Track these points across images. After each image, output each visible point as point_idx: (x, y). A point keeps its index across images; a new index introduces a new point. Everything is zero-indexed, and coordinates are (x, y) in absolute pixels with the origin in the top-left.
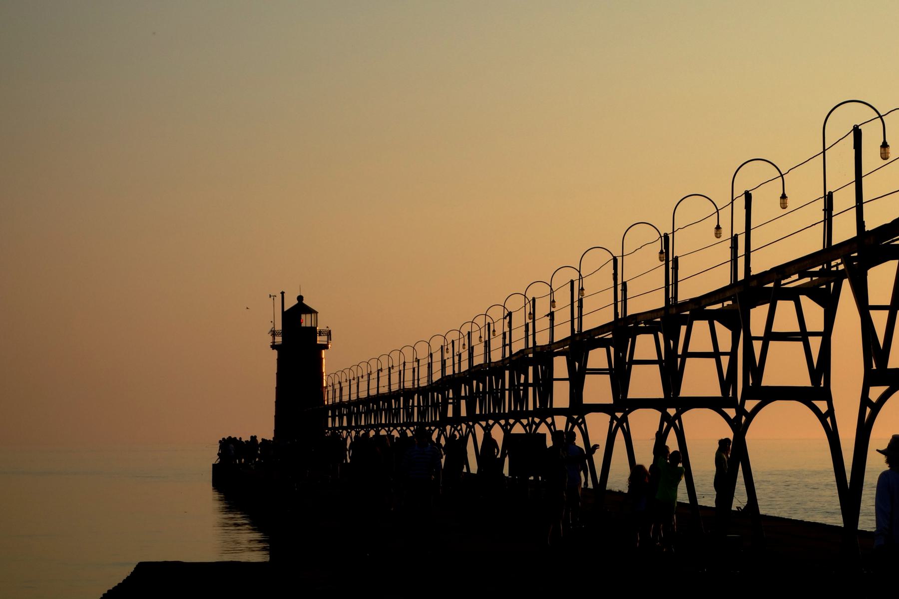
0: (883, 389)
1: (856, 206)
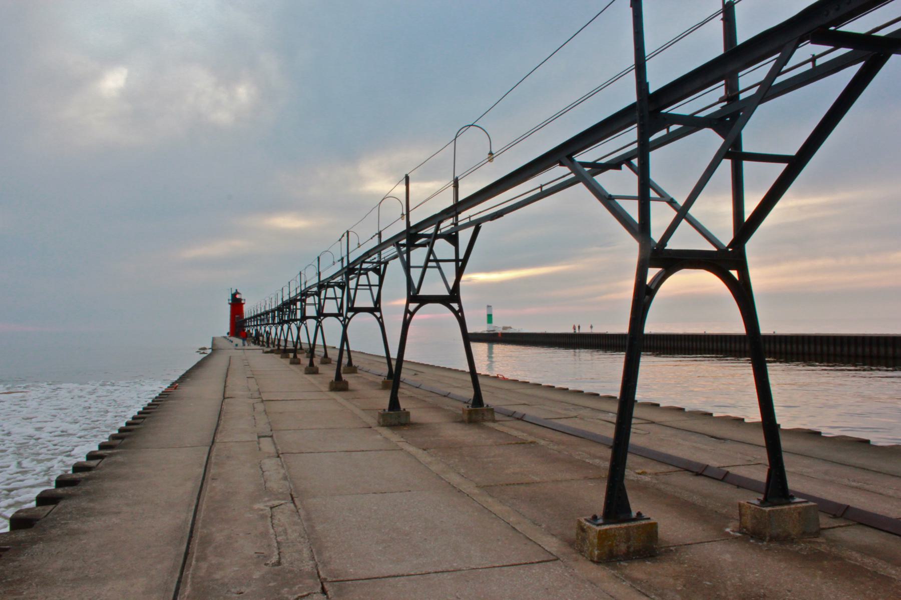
1: (644, 61)
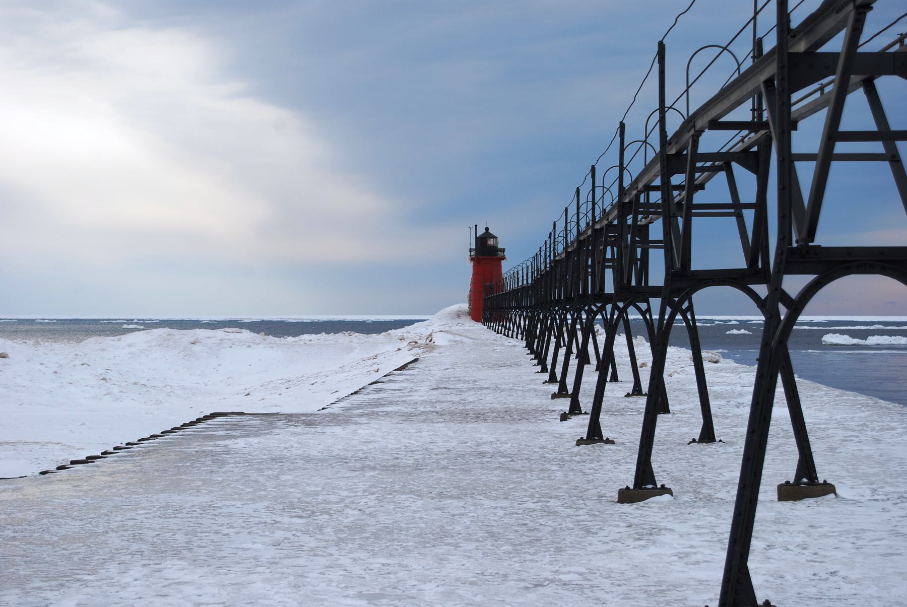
0: (809, 278)
